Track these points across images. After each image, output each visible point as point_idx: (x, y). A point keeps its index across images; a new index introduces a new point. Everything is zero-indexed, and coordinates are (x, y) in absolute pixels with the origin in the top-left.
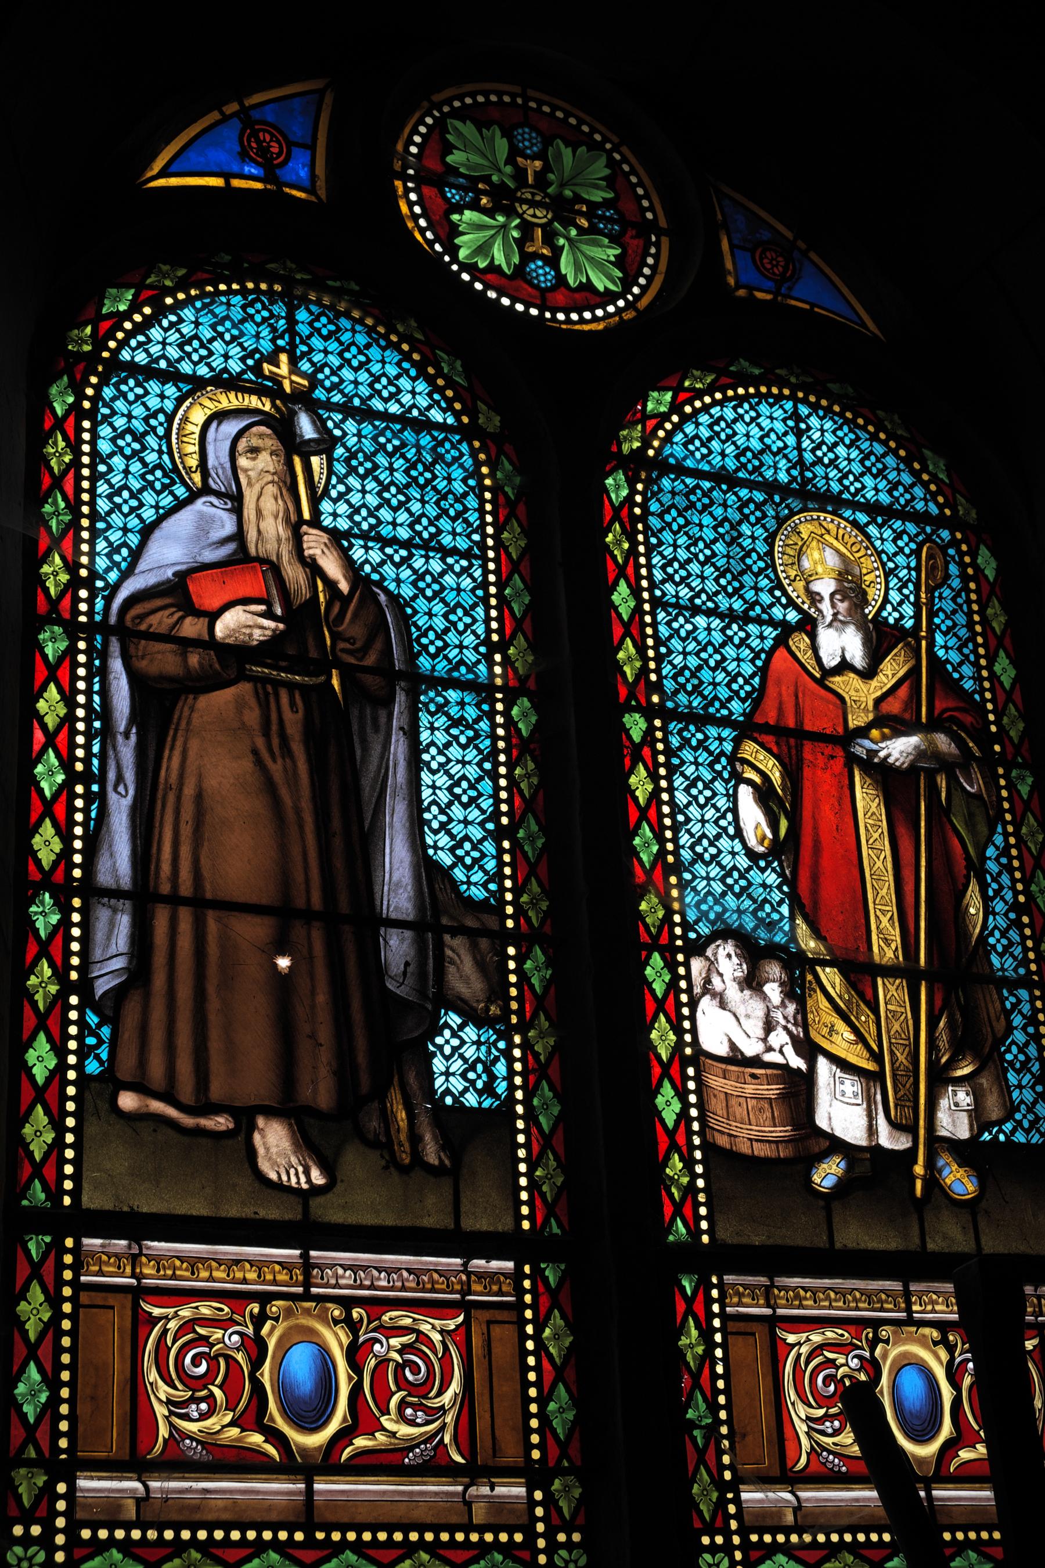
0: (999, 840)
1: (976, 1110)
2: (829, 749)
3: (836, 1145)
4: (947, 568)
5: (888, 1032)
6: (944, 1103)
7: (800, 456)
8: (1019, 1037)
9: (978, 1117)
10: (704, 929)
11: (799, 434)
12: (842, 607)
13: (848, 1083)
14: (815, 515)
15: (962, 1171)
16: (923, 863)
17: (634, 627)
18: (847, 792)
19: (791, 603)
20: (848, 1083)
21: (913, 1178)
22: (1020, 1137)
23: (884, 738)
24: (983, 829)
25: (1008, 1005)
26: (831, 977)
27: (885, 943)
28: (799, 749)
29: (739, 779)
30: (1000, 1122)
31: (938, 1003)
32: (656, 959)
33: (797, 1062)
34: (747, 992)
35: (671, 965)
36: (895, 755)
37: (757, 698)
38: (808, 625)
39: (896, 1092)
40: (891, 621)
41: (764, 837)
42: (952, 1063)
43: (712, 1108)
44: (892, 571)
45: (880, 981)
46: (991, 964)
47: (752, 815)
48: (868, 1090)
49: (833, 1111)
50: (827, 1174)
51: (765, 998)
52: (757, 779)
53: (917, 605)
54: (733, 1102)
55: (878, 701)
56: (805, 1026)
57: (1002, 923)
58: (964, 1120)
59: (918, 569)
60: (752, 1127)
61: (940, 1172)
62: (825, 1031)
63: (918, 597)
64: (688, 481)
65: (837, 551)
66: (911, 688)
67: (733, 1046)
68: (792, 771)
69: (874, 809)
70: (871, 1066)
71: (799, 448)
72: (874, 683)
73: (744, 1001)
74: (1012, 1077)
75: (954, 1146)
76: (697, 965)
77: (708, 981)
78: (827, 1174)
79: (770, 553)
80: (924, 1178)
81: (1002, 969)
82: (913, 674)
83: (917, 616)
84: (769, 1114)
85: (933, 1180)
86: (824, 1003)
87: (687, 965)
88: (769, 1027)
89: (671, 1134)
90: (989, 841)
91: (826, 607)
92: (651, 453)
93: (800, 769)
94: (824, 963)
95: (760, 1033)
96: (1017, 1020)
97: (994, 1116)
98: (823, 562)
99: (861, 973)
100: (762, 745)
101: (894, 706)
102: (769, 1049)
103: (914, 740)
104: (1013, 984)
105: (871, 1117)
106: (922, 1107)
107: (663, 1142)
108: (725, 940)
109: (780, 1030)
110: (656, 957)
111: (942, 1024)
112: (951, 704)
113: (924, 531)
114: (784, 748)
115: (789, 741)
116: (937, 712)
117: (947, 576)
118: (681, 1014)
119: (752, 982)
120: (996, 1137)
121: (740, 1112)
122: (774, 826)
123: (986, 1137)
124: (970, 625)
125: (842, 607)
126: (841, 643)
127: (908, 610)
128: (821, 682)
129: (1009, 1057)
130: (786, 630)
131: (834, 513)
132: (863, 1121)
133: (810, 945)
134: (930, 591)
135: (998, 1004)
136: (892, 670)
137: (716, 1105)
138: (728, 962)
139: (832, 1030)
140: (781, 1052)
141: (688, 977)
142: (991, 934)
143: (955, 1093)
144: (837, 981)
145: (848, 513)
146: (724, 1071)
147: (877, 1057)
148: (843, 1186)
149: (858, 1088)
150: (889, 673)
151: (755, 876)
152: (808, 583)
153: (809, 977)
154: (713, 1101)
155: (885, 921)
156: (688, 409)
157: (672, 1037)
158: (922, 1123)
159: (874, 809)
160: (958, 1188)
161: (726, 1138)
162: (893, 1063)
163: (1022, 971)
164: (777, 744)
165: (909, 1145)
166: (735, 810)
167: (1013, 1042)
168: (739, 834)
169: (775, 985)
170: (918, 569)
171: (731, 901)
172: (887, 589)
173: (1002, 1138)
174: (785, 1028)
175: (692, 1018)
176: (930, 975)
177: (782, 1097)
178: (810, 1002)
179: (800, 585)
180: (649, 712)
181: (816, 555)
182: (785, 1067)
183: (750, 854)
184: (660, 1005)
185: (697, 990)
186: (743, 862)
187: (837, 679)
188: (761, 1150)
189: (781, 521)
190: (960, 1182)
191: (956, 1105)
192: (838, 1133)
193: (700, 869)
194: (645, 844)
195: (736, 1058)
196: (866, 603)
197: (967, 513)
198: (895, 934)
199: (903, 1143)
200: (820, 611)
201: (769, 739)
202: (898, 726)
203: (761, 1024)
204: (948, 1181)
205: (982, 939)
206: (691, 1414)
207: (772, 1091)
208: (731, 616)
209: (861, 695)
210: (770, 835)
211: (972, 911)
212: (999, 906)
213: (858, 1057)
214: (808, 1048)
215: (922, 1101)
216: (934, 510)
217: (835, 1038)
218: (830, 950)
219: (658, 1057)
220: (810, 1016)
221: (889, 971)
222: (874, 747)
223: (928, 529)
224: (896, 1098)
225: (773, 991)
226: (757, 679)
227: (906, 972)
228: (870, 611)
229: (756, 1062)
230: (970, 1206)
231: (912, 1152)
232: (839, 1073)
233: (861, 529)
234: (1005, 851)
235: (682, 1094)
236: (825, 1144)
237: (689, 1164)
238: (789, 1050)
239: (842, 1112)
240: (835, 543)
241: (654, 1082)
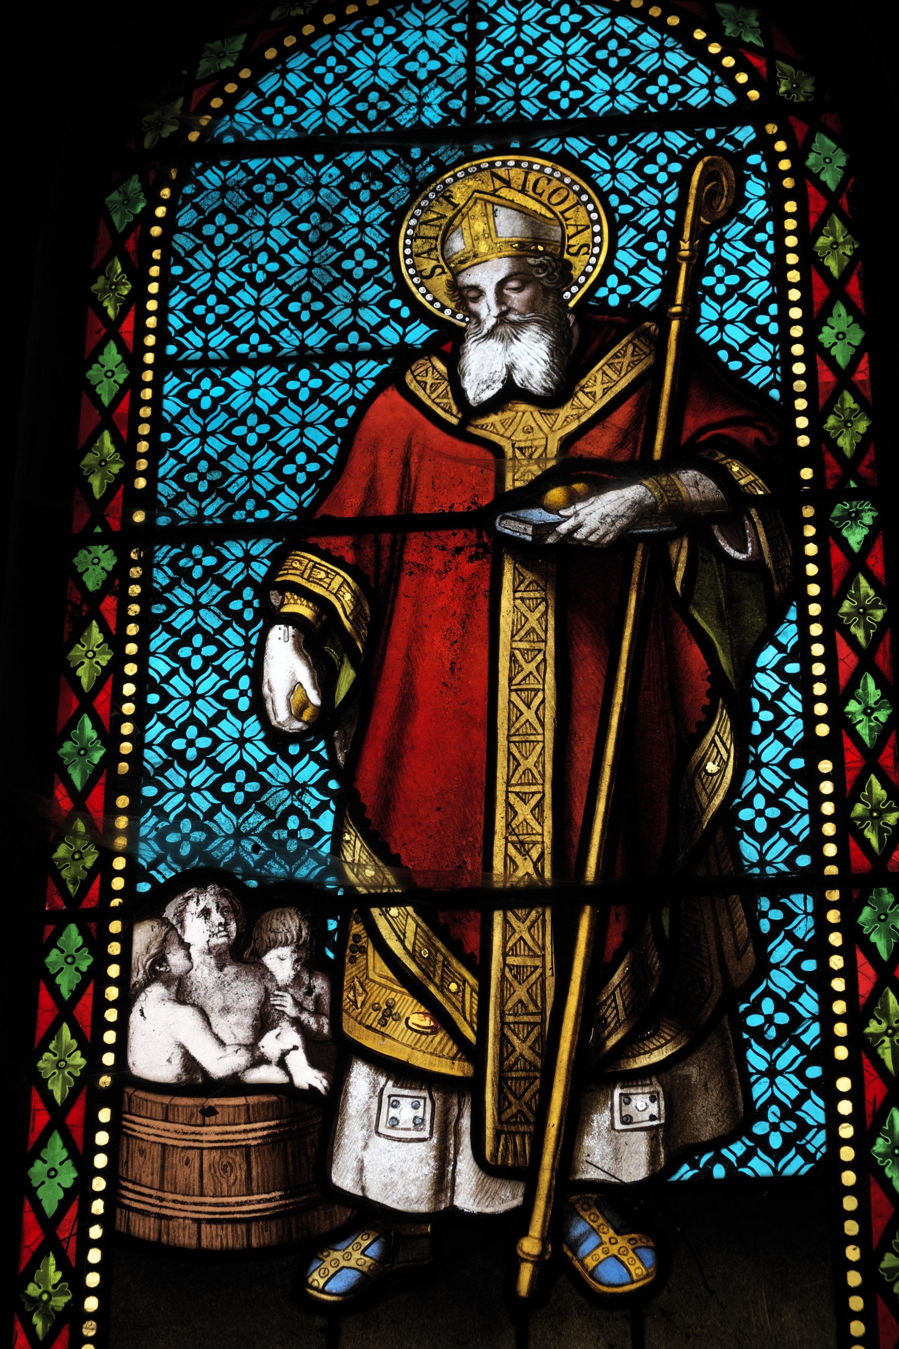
0: (788, 634)
1: (666, 1126)
2: (457, 538)
3: (365, 1214)
4: (741, 188)
5: (502, 1003)
6: (600, 1120)
7: (471, 74)
8: (783, 981)
9: (672, 1140)
10: (165, 873)
11: (472, 41)
12: (517, 299)
13: (405, 1103)
14: (484, 163)
15: (622, 1241)
16: (619, 698)
17: (120, 419)
18: (483, 604)
19: (420, 313)
20: (405, 1103)
21: (515, 1262)
22: (760, 1166)
23: (572, 499)
24: (756, 621)
25: (765, 926)
26: (399, 927)
27: (521, 841)
28: (398, 548)
29: (271, 616)
30: (719, 1143)
31: (614, 940)
32: (73, 936)
33: (306, 1076)
34: (230, 970)
35: (96, 942)
36: (592, 522)
37: (327, 484)
38: (449, 344)
39: (500, 1109)
40: (614, 301)
41: (306, 703)
42: (632, 1043)
43: (133, 1173)
44: (625, 219)
45: (498, 917)
46: (738, 856)
47: (286, 668)
48: (446, 1112)
49: (367, 1157)
50: (338, 1271)
51: (264, 973)
52: (304, 609)
53: (670, 267)
54: (175, 1159)
55: (567, 442)
56: (336, 1015)
57: (772, 779)
58: (640, 1145)
59: (680, 206)
60: (208, 1198)
61: (575, 1246)
62: (373, 1018)
63: (673, 250)
64: (253, 164)
65: (521, 210)
66: (639, 406)
67: (190, 1063)
68: (376, 593)
69: (533, 622)
70: (457, 1069)
71: (470, 63)
72: (566, 411)
73: (222, 985)
74: (756, 1059)
75: (614, 1198)
76: (144, 936)
77: (160, 958)
78: (338, 1271)
79: (391, 244)
80: (538, 1262)
81: (762, 863)
82: (649, 381)
83: (668, 285)
84: (241, 1174)
85: (558, 1262)
86: (378, 967)
87: (126, 938)
88: (264, 1021)
89: (49, 1224)
90: (769, 638)
91: (487, 310)
92: (194, 136)
93: (393, 579)
94: (386, 901)
95: (244, 1035)
96: (782, 951)
97: (706, 1134)
98: (490, 234)
99: (458, 907)
100: (325, 555)
101: (598, 445)
102: (259, 1061)
103: (633, 492)
104: (780, 887)
105: (444, 1161)
106: (554, 1119)
107: (33, 1236)
108: (202, 887)
109: (285, 1025)
110: (73, 930)
111: (616, 979)
112: (718, 416)
113: (701, 138)
114: (369, 553)
115: (377, 543)
116: (685, 436)
117: (741, 200)
118: (98, 1019)
119: (242, 952)
120: (707, 1170)
121: (185, 1174)
122: (325, 680)
123: (685, 1172)
124: (777, 276)
125: (517, 299)
126: (507, 356)
127: (652, 275)
128: (460, 432)
129: (754, 1021)
130: (404, 356)
131: (525, 150)
132: (428, 1170)
133: (361, 865)
134: (701, 235)
135: (743, 928)
136: (601, 385)
137: (143, 1169)
138: (201, 925)
139: (389, 1013)
140: (282, 1064)
141: (125, 959)
142: (748, 802)
143: (626, 1099)
144: (411, 927)
145: (550, 145)
146: (167, 1108)
147: (474, 1053)
148: (367, 1291)
149: (425, 1111)
150: (598, 389)
151: (279, 773)
152: (456, 274)
153: (357, 928)
154: (138, 1160)
155: (524, 811)
156: (844, 1084)
157: (78, 1060)
158: (547, 1160)
159: (533, 622)
160: (611, 1273)
161: (151, 1222)
162: (501, 1059)
163: (804, 861)
164: (356, 547)
165: (517, 1202)
166: (256, 674)
167: (768, 993)
168: (259, 706)
169: (286, 951)
170: (680, 206)
171: (225, 820)
172: (613, 249)
173: (719, 1172)
174: (296, 1022)
175: (122, 1027)
176: (601, 896)
177: (271, 1141)
178: (350, 972)
179: (440, 282)
180: (123, 540)
181: (479, 226)
182: (288, 1089)
183: (276, 738)
184: (66, 1011)
185: (138, 977)
186: (257, 752)
187: (493, 418)
188: (213, 1238)
189: (416, 188)
190: (614, 1260)
191: (627, 1120)
192: (374, 1194)
193: (176, 777)
194: (82, 749)
195: (195, 1082)
196: (568, 280)
197: (796, 87)
198: (544, 832)
199: (505, 1199)
200: (475, 316)
201: (342, 544)
202: (597, 476)
203: (248, 1020)
204: (590, 1262)
205: (728, 812)
206: (32, 1290)
207: (254, 1132)
208: (304, 357)
209: (531, 438)
210: (314, 698)
211: (711, 767)
212: (772, 750)
213: (436, 1057)
214: (334, 1052)
215: (554, 1119)
216: (725, 96)
217: (396, 1029)
218: (404, 877)
219: (48, 1096)
220: (348, 995)
221: (518, 898)
222: (551, 518)
223: (711, 134)
224: (499, 1120)
225: (281, 963)
226: (333, 450)
227: (558, 897)
228: (573, 296)
229: (233, 1085)
230: (632, 1305)
231: (518, 1220)
232: (390, 1088)
233: (575, 164)
234: (801, 652)
235: (82, 1156)
236: (342, 1215)
237: (73, 1274)
238: (298, 1063)
239: (387, 1155)
240: (519, 198)
241: (26, 1257)
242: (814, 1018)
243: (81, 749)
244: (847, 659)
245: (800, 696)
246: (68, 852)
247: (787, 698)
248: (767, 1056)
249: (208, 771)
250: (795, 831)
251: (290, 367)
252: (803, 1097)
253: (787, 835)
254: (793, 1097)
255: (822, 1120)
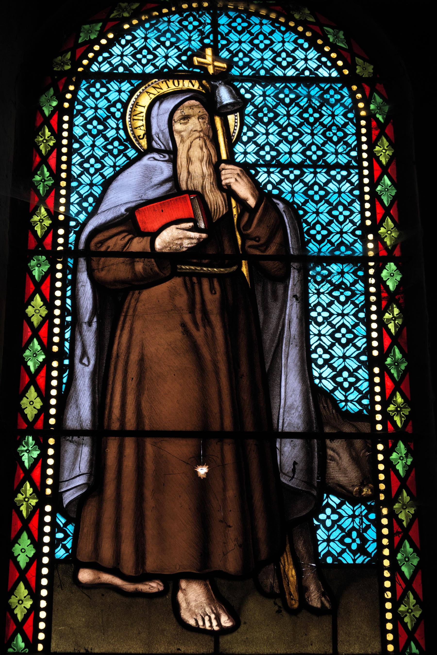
242: (72, 204)
243: (409, 558)
244: (52, 161)
245: (72, 172)
246: (388, 273)
247: (76, 211)
248: (92, 191)
249: (329, 327)
250: (78, 157)
251: (274, 162)
252: (80, 176)
253: (82, 156)
254: (84, 176)
255: (71, 206)
